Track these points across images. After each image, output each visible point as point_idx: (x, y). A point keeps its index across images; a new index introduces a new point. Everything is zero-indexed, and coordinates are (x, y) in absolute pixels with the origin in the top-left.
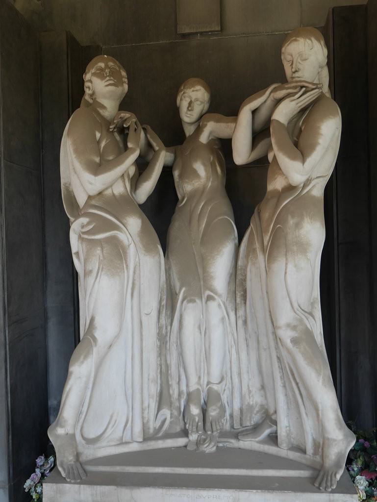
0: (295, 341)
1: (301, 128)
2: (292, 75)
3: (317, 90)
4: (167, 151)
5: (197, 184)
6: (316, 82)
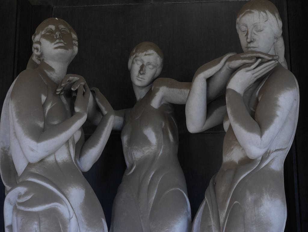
1: (257, 99)
2: (247, 45)
3: (273, 62)
4: (116, 114)
5: (147, 151)
6: (271, 52)
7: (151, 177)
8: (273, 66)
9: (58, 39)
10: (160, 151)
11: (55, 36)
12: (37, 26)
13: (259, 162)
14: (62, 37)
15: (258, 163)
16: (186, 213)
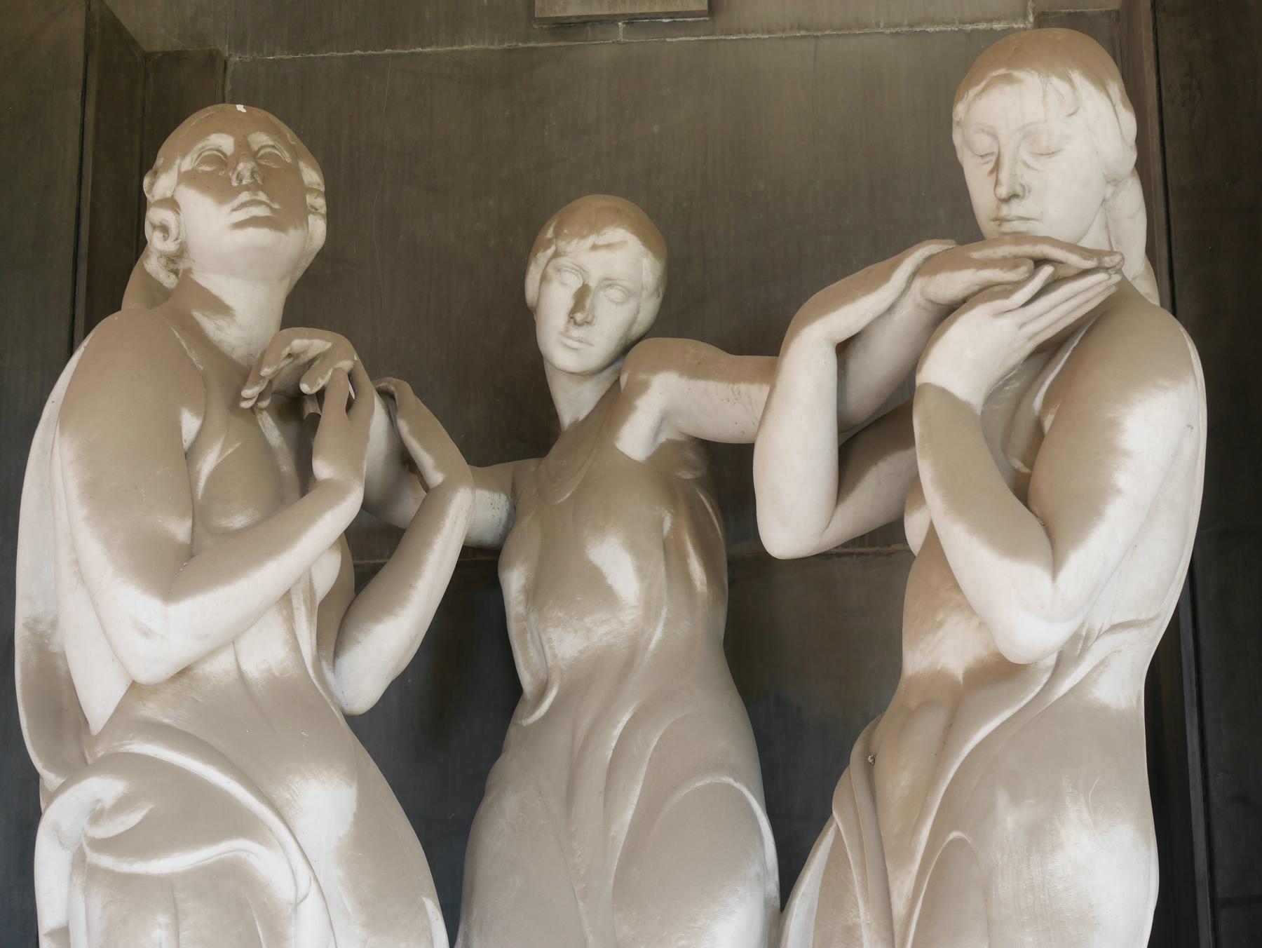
2: (998, 208)
4: (479, 484)
5: (603, 630)
9: (247, 188)
11: (234, 177)
14: (260, 182)
15: (1044, 680)
16: (758, 875)
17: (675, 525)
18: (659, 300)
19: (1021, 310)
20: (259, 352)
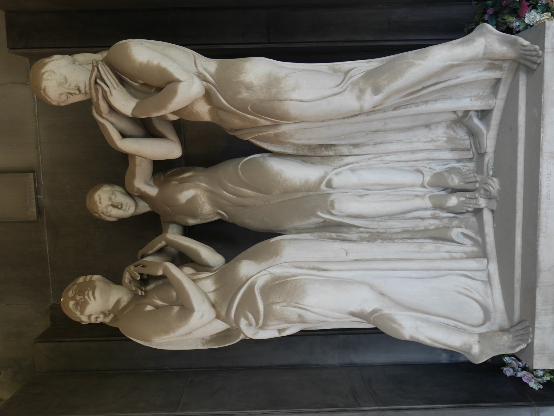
0: (376, 91)
2: (82, 94)
3: (99, 66)
4: (167, 232)
5: (203, 199)
7: (228, 195)
8: (105, 67)
9: (84, 297)
10: (202, 185)
11: (81, 300)
12: (70, 319)
13: (208, 84)
14: (82, 293)
15: (210, 85)
16: (263, 159)
17: (176, 181)
18: (115, 185)
19: (110, 88)
20: (130, 291)
